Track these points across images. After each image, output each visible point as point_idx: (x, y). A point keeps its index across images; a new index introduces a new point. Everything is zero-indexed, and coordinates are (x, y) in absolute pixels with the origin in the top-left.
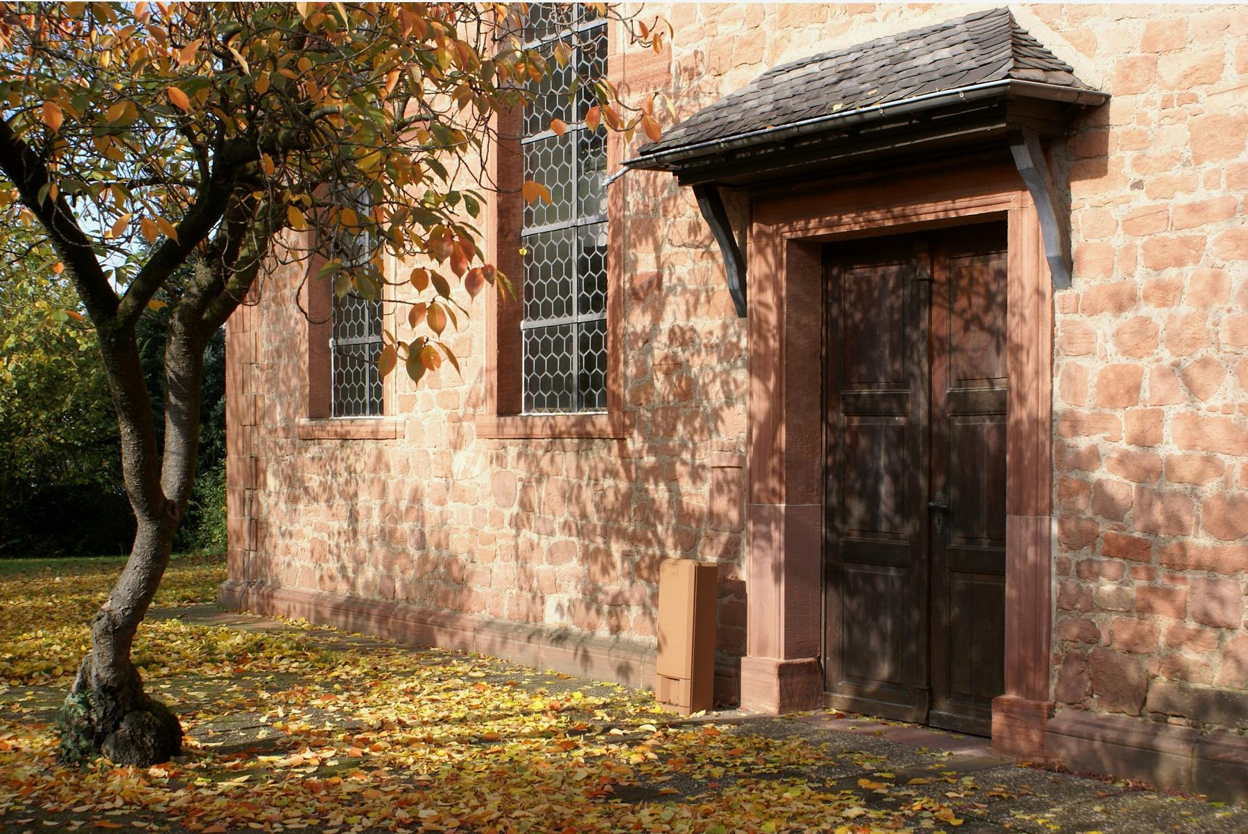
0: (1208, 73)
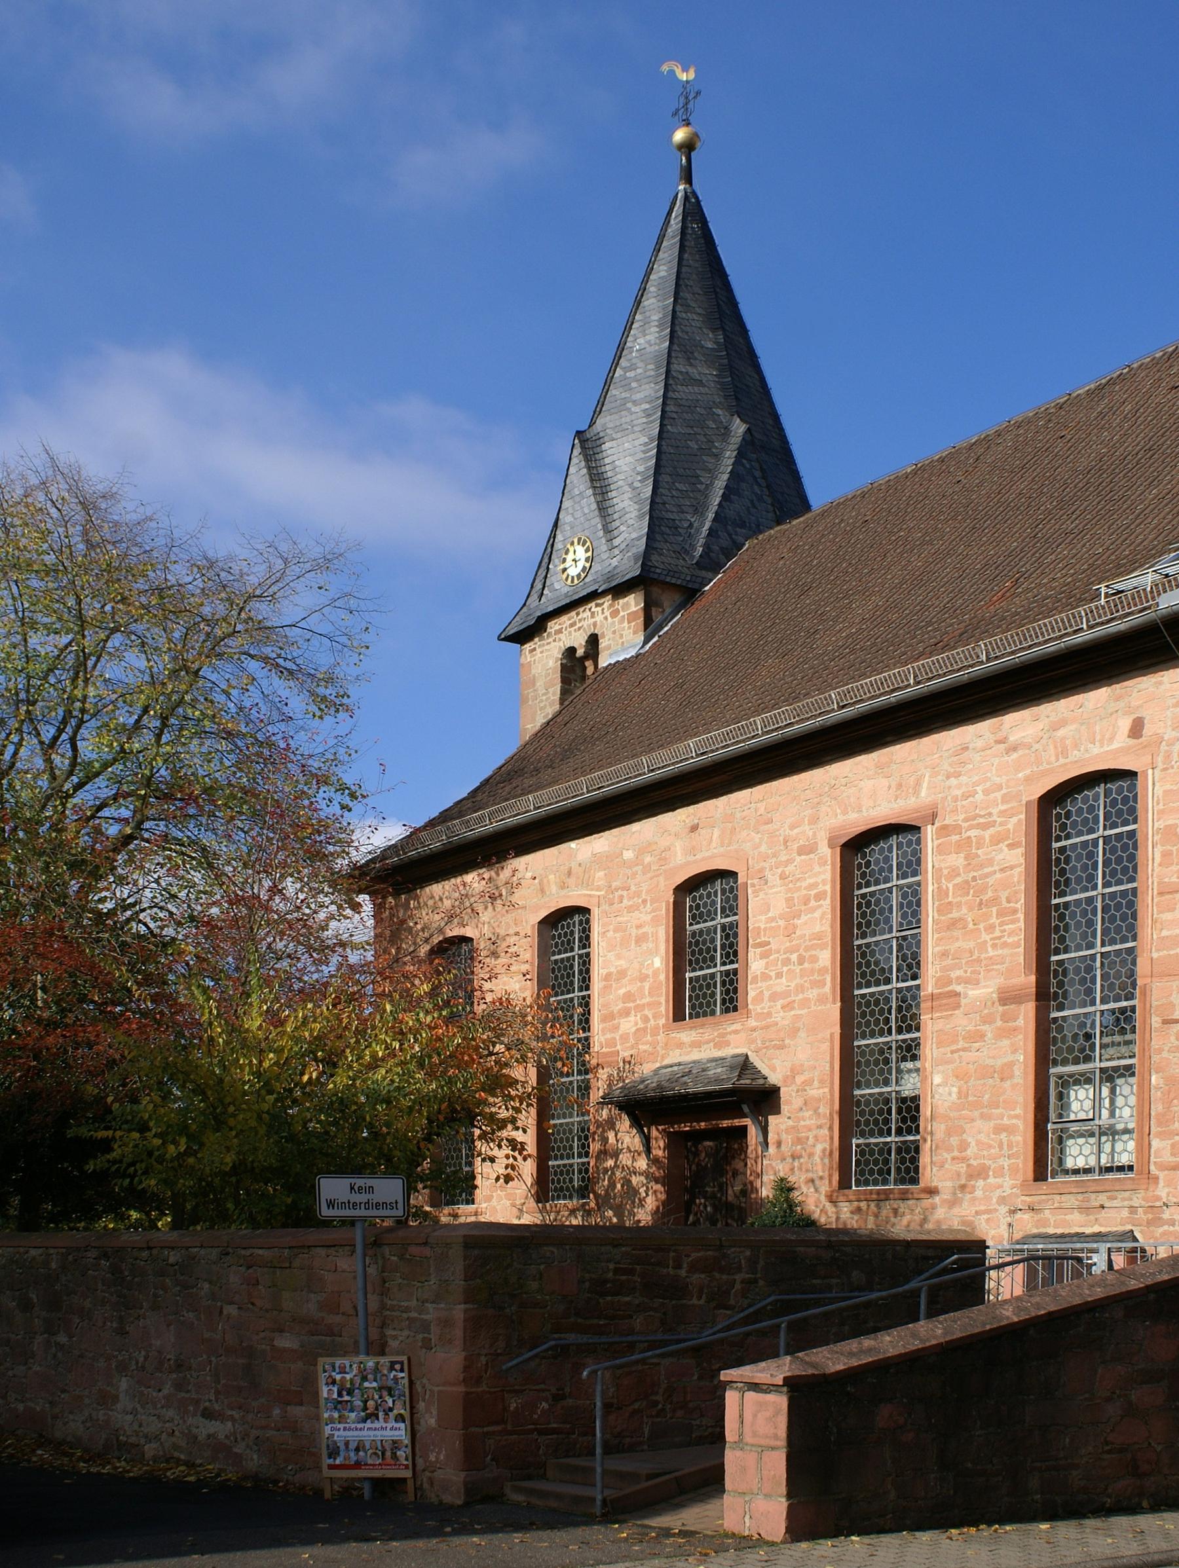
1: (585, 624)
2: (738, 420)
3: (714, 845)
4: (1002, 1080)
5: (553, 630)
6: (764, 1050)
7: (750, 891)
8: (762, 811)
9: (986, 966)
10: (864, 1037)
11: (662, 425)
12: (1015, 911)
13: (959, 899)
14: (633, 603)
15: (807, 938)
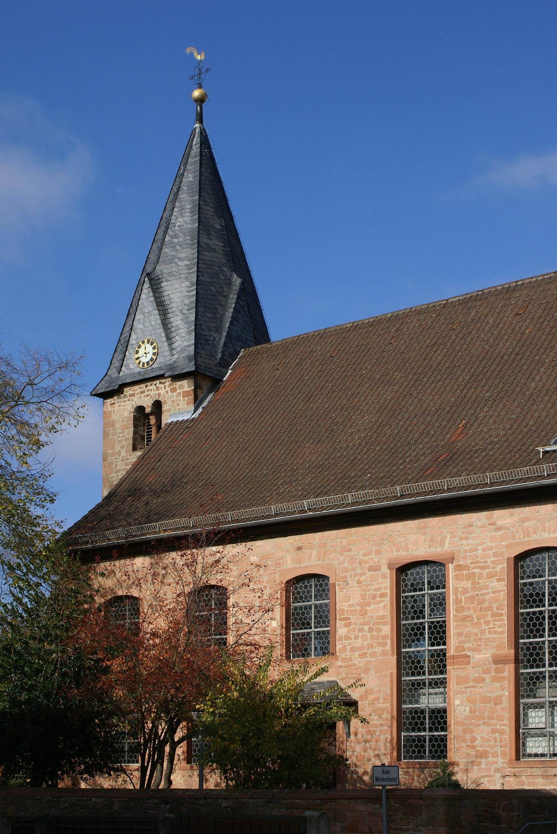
0: (377, 699)
1: (152, 393)
2: (235, 276)
4: (496, 704)
5: (128, 394)
6: (347, 680)
8: (345, 543)
9: (485, 642)
10: (408, 675)
11: (198, 276)
12: (501, 615)
13: (468, 605)
14: (186, 385)
15: (375, 618)
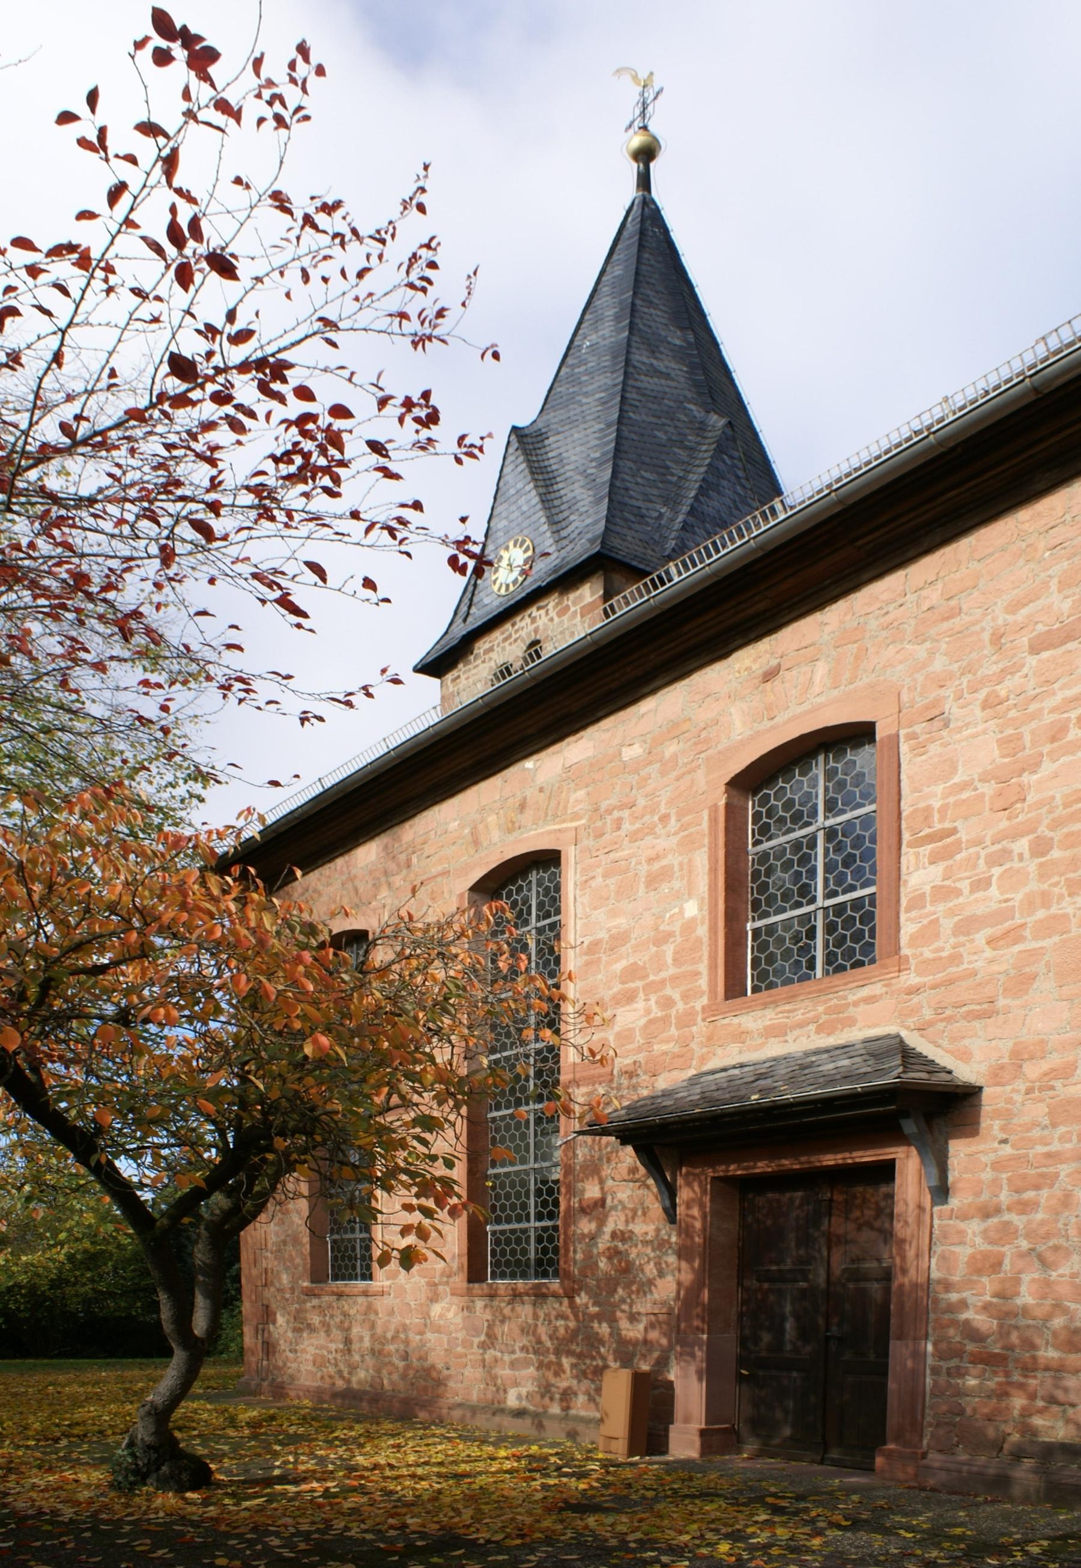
1: (523, 633)
3: (817, 689)
6: (941, 1026)
7: (904, 748)
